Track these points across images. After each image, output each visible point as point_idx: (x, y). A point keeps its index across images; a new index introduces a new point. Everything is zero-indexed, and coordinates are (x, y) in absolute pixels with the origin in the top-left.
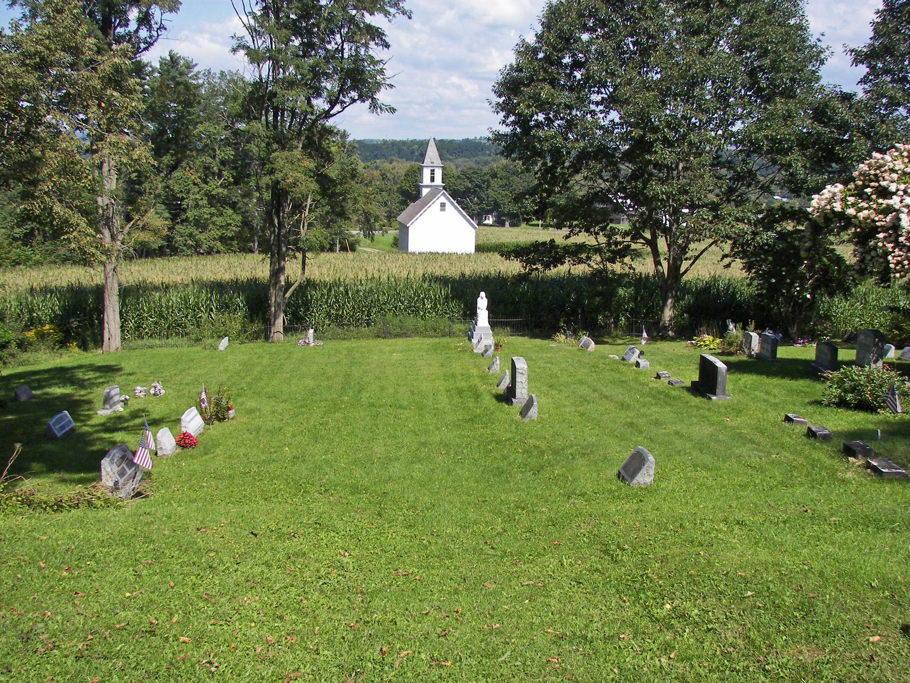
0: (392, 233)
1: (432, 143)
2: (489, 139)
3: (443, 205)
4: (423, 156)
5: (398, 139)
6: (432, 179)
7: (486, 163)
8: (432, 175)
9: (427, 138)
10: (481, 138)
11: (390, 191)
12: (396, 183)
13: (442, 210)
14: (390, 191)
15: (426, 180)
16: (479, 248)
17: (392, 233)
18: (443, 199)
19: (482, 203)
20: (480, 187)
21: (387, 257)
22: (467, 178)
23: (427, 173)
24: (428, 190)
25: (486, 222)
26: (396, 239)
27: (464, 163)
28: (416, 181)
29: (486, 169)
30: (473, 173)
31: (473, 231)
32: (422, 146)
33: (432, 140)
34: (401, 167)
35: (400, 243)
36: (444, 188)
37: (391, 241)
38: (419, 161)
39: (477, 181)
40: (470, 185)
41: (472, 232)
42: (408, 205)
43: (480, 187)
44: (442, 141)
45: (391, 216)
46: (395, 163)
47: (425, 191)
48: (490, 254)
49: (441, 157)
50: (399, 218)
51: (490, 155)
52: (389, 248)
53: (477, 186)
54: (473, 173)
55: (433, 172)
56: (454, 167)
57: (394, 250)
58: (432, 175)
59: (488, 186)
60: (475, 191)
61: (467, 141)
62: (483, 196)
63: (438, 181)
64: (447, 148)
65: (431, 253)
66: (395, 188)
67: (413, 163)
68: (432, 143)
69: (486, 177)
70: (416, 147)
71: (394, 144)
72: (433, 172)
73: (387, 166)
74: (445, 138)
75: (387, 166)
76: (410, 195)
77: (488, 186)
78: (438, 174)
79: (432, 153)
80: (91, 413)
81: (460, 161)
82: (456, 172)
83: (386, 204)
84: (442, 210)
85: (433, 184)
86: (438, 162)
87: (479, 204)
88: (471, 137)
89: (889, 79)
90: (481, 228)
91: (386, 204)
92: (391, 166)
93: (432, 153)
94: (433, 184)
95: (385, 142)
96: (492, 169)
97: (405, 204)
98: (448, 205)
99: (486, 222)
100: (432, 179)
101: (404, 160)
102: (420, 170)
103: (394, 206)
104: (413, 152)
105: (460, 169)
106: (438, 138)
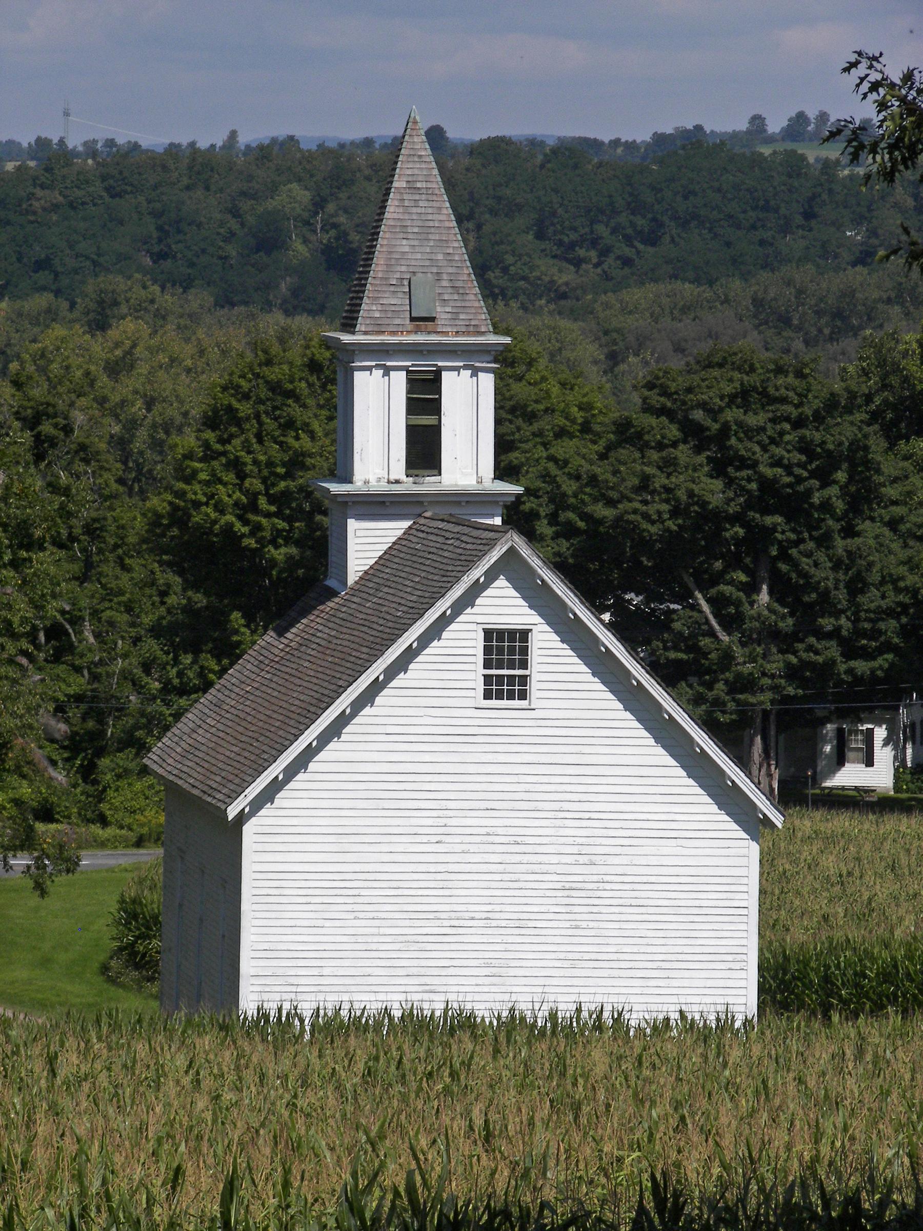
0: (114, 866)
1: (417, 169)
2: (857, 140)
3: (505, 651)
4: (347, 265)
5: (153, 139)
6: (424, 449)
7: (842, 319)
8: (419, 426)
9: (384, 129)
10: (797, 126)
11: (88, 545)
12: (137, 480)
13: (494, 689)
14: (88, 545)
15: (377, 452)
16: (788, 983)
17: (114, 866)
18: (503, 605)
19: (807, 626)
20: (795, 506)
21: (70, 1062)
22: (693, 432)
23: (377, 405)
24: (392, 530)
25: (850, 776)
26: (136, 919)
27: (669, 323)
28: (297, 463)
29: (839, 368)
30: (742, 397)
31: (745, 855)
32: (352, 181)
33: (418, 144)
34: (178, 355)
35: (179, 938)
36: (518, 517)
37: (103, 932)
38: (316, 311)
39: (773, 460)
40: (714, 492)
41: (737, 860)
42: (229, 652)
43: (795, 506)
44: (495, 150)
45: (98, 740)
46: (126, 328)
47: (366, 544)
48: (876, 1031)
49: (493, 273)
50: (166, 755)
51: (864, 258)
52: (82, 991)
53: (769, 496)
54: (742, 397)
55: (424, 397)
56: (587, 351)
57: (131, 1003)
58: (419, 426)
59: (862, 498)
60: (759, 538)
61: (688, 150)
62: (824, 574)
63: (468, 458)
64: (542, 214)
65: (415, 1025)
66: (132, 517)
67: (272, 322)
68: (417, 169)
69: (844, 431)
70: (295, 196)
71: (123, 173)
72: (424, 397)
73: (72, 345)
74: (515, 127)
75: (72, 345)
76: (250, 587)
77: (862, 498)
78: (469, 406)
79: (419, 243)
80: (358, 301)
81: (639, 303)
82: (611, 397)
83: (58, 641)
84: (494, 689)
85: (429, 484)
86: (463, 313)
87: (786, 642)
88: (725, 120)
89: (543, 302)
90: (810, 821)
91: (58, 641)
92: (100, 347)
93: (419, 243)
94: (429, 484)
95: (51, 158)
96: (886, 367)
97: (205, 642)
98: (545, 642)
99: (850, 776)
100: (424, 449)
101: (200, 298)
102: (329, 379)
103: (121, 657)
104: (268, 241)
105: (635, 368)
106: (464, 130)
